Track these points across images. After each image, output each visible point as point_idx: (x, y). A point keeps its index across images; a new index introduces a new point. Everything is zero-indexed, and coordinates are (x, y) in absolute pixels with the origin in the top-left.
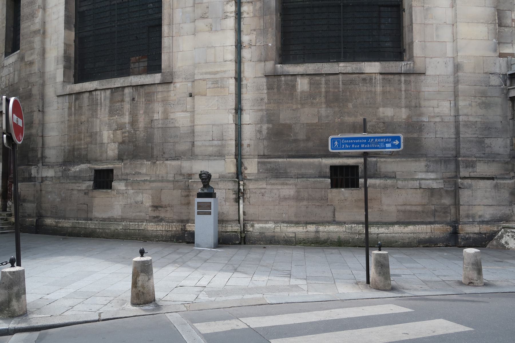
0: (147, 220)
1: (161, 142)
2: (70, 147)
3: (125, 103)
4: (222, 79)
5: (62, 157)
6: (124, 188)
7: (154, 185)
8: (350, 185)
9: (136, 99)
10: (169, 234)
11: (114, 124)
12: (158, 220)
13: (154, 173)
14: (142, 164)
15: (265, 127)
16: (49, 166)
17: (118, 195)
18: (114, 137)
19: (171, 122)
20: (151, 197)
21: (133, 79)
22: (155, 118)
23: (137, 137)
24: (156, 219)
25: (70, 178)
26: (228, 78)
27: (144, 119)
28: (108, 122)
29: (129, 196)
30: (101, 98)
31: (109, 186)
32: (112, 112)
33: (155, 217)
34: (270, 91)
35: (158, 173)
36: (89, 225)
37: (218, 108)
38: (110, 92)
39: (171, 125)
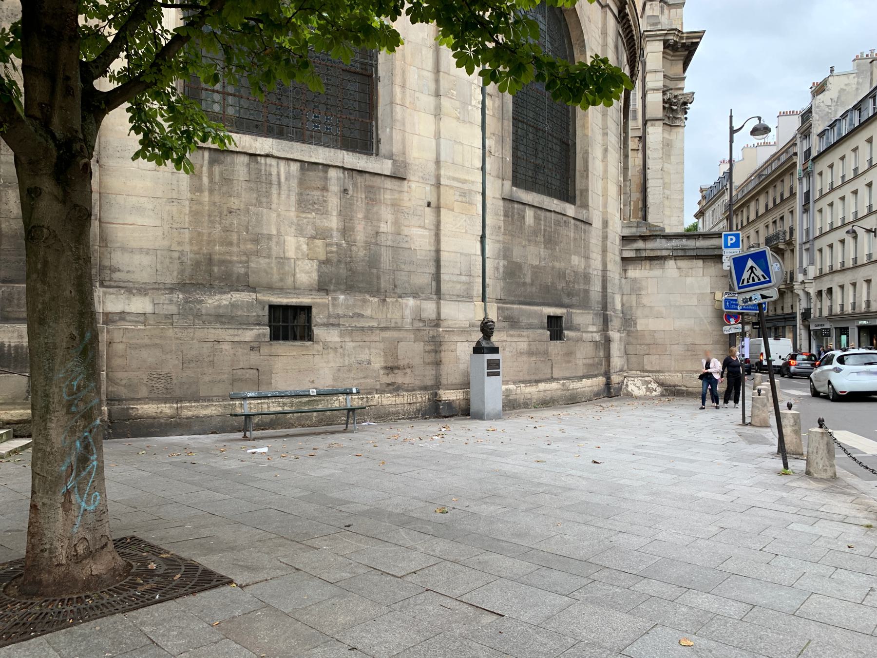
0: (377, 390)
1: (391, 268)
2: (197, 256)
3: (329, 194)
4: (470, 191)
5: (175, 273)
6: (338, 339)
7: (387, 334)
8: (281, 337)
9: (350, 192)
10: (413, 408)
11: (309, 227)
12: (395, 388)
13: (384, 316)
14: (365, 301)
15: (502, 263)
16: (131, 289)
17: (326, 352)
18: (309, 249)
19: (405, 240)
20: (383, 354)
21: (346, 156)
22: (382, 230)
23: (353, 256)
24: (391, 387)
25: (204, 317)
26: (476, 192)
27: (364, 228)
28: (296, 221)
29: (346, 352)
30: (278, 175)
31: (305, 334)
32: (303, 204)
33: (389, 385)
34: (506, 219)
35: (389, 316)
36: (269, 407)
37: (466, 232)
38: (299, 168)
39: (405, 245)
